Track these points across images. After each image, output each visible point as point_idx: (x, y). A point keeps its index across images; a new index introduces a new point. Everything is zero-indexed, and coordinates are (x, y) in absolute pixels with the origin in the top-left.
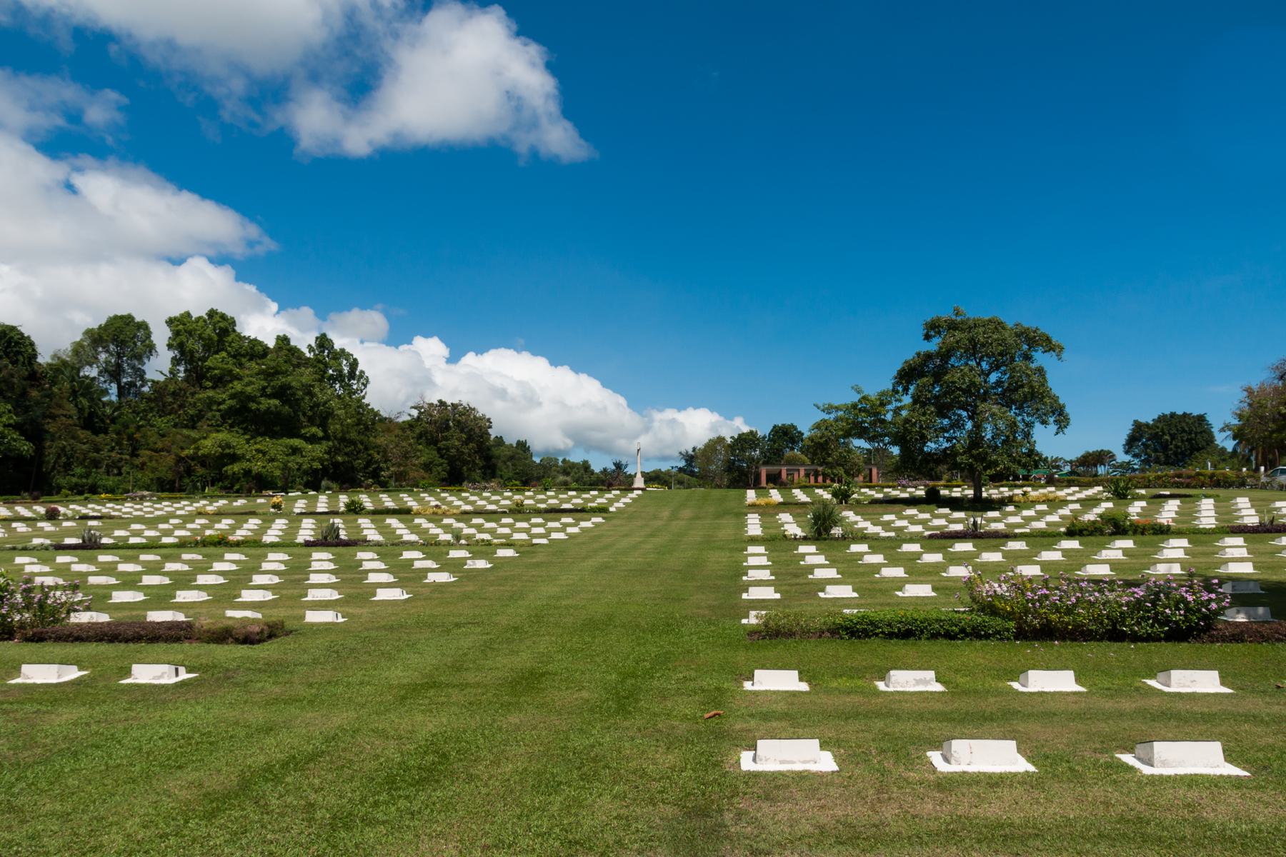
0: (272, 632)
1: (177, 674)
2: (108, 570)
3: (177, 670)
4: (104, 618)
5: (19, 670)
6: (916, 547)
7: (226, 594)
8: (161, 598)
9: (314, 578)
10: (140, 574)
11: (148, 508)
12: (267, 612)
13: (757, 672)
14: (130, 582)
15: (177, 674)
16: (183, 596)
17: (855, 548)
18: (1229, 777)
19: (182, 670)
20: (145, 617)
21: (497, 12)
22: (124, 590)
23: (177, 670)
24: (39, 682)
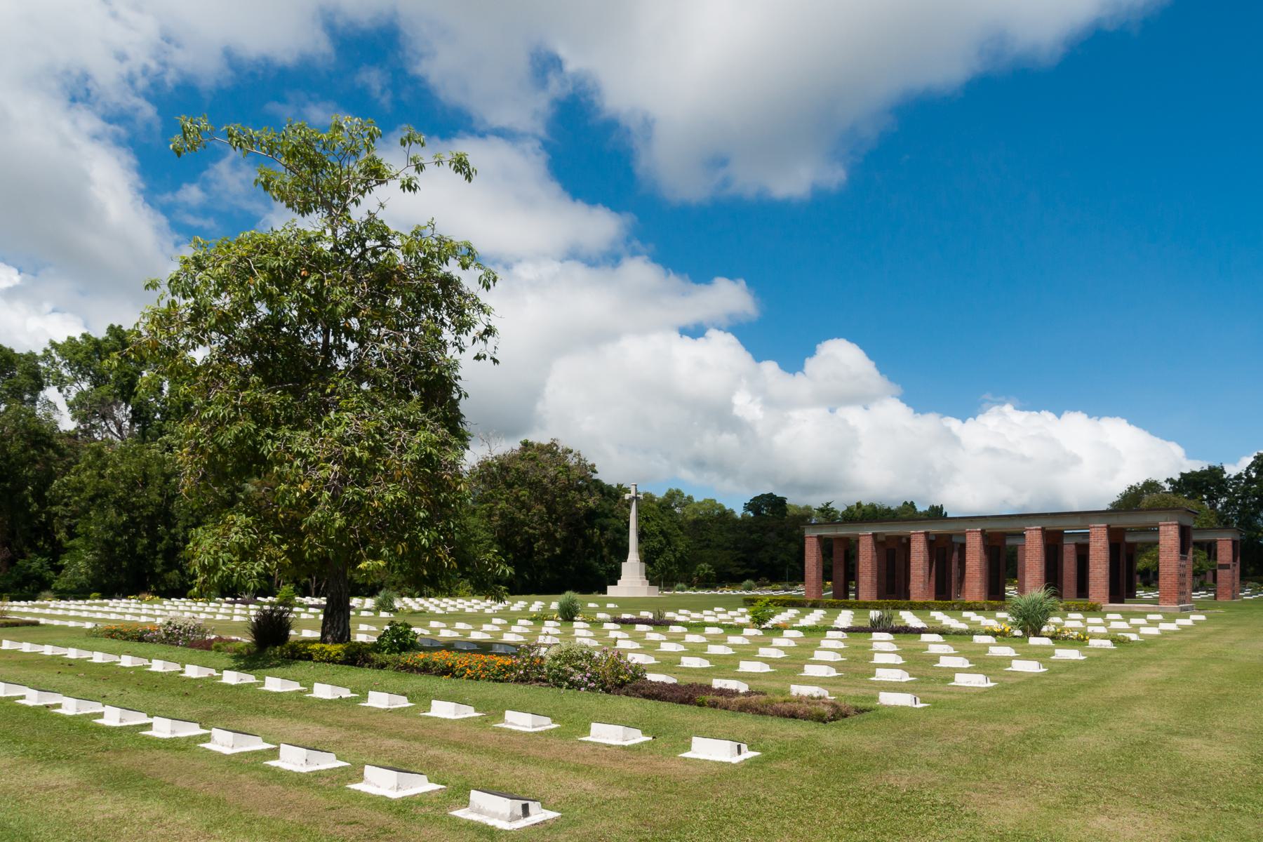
0: (838, 714)
1: (739, 752)
2: (677, 639)
3: (739, 747)
4: (670, 680)
5: (502, 716)
6: (989, 639)
7: (791, 666)
8: (725, 666)
9: (878, 659)
10: (706, 644)
11: (53, 604)
12: (752, 683)
13: (594, 725)
14: (694, 651)
15: (739, 752)
16: (746, 666)
17: (978, 639)
18: (544, 822)
19: (744, 747)
20: (876, 699)
21: (807, 360)
22: (949, 668)
23: (739, 747)
24: (702, 757)
